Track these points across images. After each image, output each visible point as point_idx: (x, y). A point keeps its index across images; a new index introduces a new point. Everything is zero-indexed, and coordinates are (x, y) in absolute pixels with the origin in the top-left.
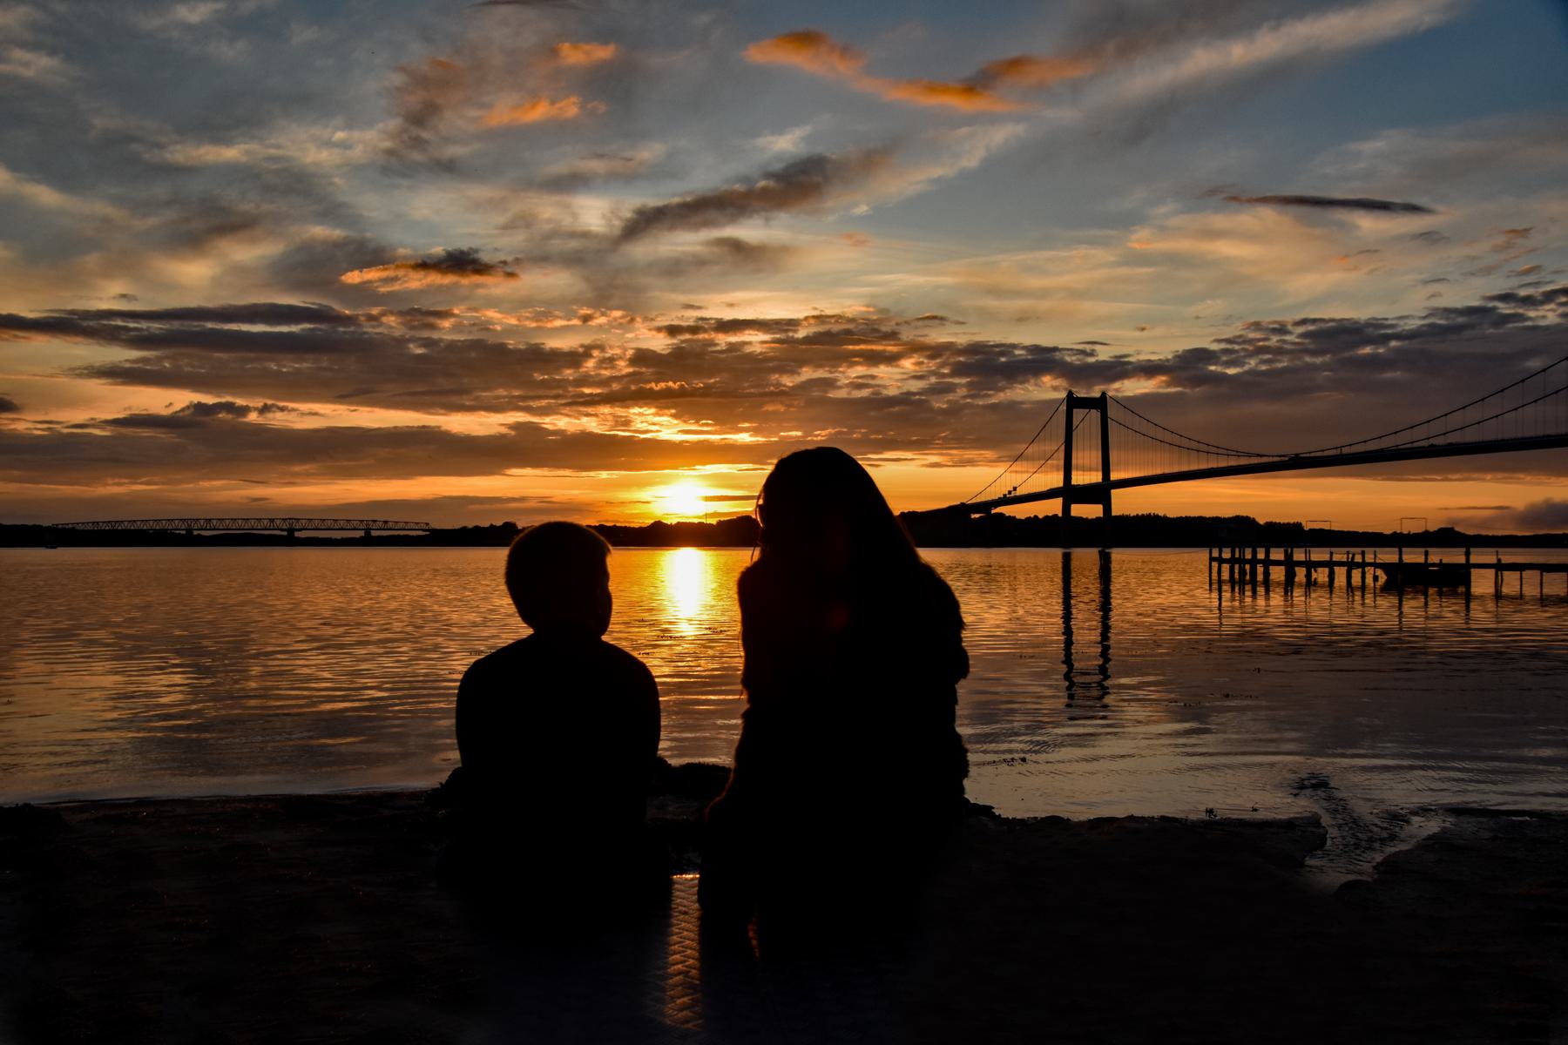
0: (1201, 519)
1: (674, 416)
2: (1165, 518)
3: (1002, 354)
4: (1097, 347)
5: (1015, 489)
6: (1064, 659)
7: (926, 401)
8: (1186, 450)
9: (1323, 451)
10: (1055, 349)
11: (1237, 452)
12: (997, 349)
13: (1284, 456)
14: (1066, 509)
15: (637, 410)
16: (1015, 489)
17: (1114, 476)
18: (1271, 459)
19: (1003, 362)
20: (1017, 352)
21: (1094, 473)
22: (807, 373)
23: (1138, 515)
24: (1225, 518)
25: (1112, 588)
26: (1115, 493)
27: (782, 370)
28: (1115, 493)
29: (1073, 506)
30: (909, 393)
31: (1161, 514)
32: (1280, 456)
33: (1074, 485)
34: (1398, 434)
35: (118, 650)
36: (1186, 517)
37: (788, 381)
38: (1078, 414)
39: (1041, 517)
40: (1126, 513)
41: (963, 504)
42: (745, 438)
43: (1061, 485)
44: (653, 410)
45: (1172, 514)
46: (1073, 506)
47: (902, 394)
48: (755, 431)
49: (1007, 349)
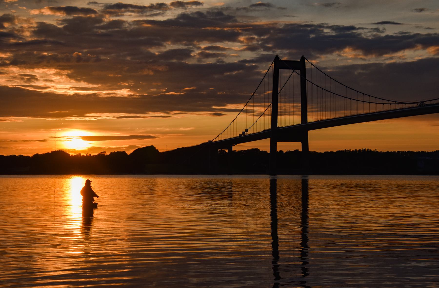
0: (410, 153)
1: (70, 76)
2: (376, 153)
3: (312, 32)
4: (386, 26)
5: (247, 130)
6: (275, 278)
7: (256, 67)
8: (344, 98)
9: (431, 100)
10: (353, 28)
11: (389, 101)
12: (309, 29)
13: (414, 103)
14: (273, 146)
15: (41, 71)
16: (247, 130)
17: (311, 119)
18: (404, 106)
19: (313, 38)
20: (326, 30)
21: (296, 117)
22: (169, 46)
23: (131, 153)
24: (428, 153)
25: (270, 218)
26: (311, 133)
27: (151, 44)
28: (311, 133)
29: (279, 144)
30: (245, 61)
31: (373, 150)
32: (410, 103)
33: (279, 127)
34: (286, 84)
35: (253, 238)
36: (325, 153)
37: (155, 51)
38: (285, 74)
39: (285, 151)
40: (348, 149)
41: (210, 142)
42: (124, 93)
43: (269, 127)
44: (53, 71)
45: (415, 151)
46: (279, 144)
47: (239, 61)
48: (131, 88)
49: (316, 29)
